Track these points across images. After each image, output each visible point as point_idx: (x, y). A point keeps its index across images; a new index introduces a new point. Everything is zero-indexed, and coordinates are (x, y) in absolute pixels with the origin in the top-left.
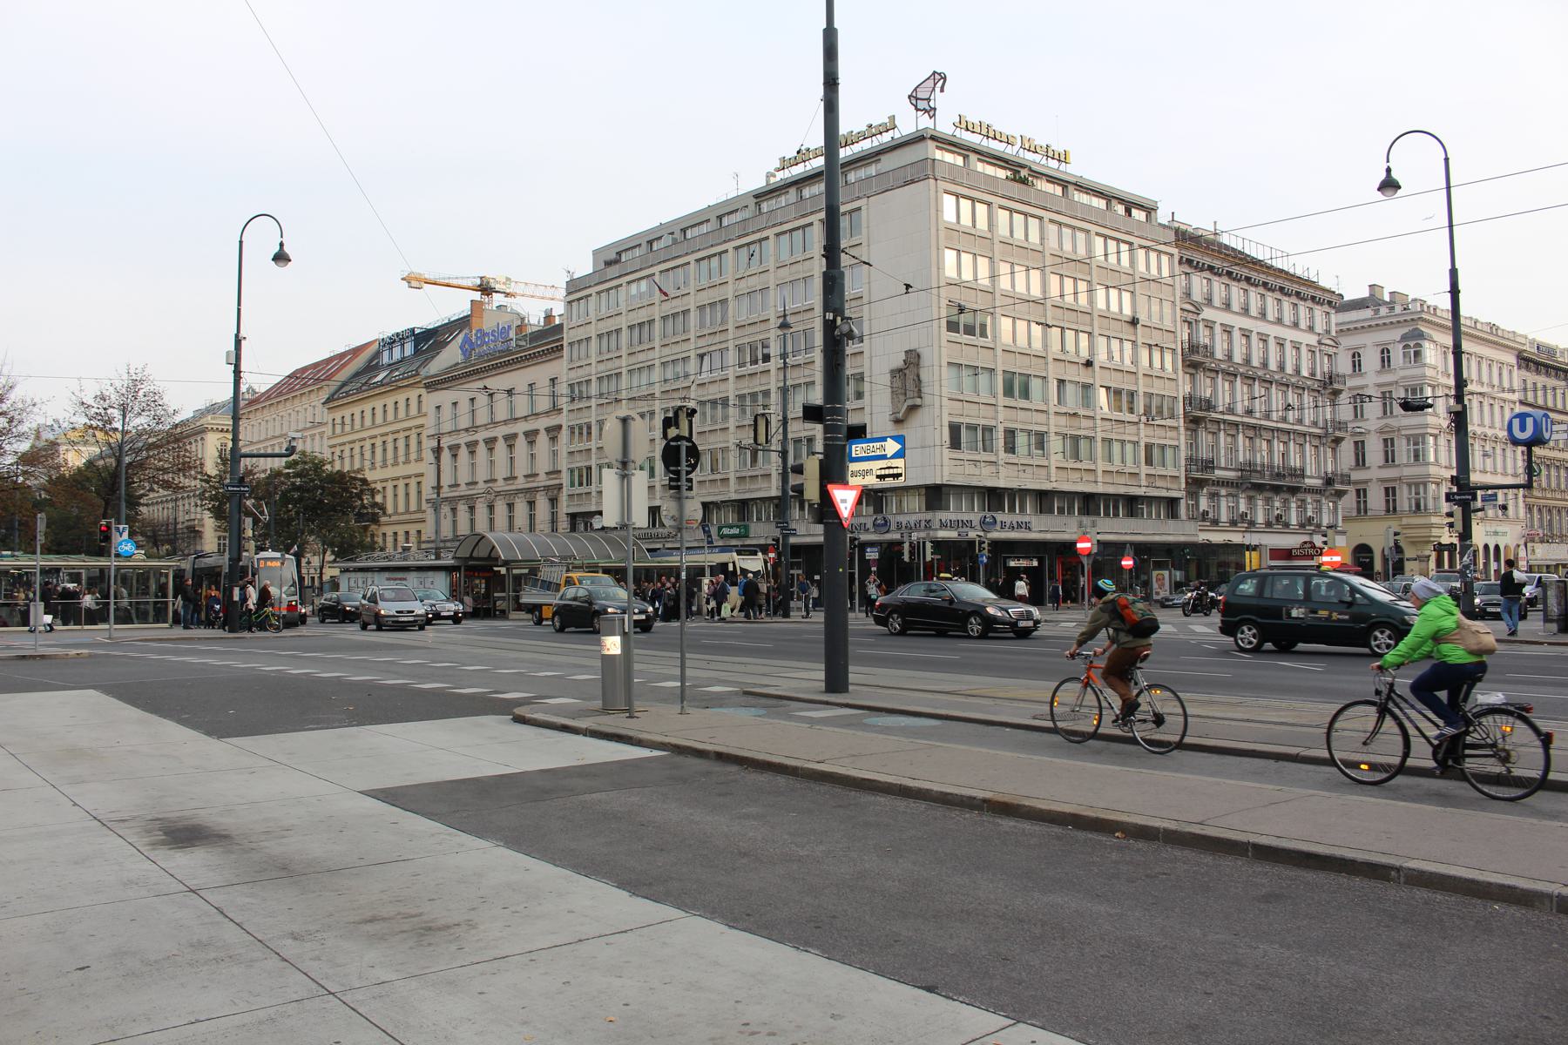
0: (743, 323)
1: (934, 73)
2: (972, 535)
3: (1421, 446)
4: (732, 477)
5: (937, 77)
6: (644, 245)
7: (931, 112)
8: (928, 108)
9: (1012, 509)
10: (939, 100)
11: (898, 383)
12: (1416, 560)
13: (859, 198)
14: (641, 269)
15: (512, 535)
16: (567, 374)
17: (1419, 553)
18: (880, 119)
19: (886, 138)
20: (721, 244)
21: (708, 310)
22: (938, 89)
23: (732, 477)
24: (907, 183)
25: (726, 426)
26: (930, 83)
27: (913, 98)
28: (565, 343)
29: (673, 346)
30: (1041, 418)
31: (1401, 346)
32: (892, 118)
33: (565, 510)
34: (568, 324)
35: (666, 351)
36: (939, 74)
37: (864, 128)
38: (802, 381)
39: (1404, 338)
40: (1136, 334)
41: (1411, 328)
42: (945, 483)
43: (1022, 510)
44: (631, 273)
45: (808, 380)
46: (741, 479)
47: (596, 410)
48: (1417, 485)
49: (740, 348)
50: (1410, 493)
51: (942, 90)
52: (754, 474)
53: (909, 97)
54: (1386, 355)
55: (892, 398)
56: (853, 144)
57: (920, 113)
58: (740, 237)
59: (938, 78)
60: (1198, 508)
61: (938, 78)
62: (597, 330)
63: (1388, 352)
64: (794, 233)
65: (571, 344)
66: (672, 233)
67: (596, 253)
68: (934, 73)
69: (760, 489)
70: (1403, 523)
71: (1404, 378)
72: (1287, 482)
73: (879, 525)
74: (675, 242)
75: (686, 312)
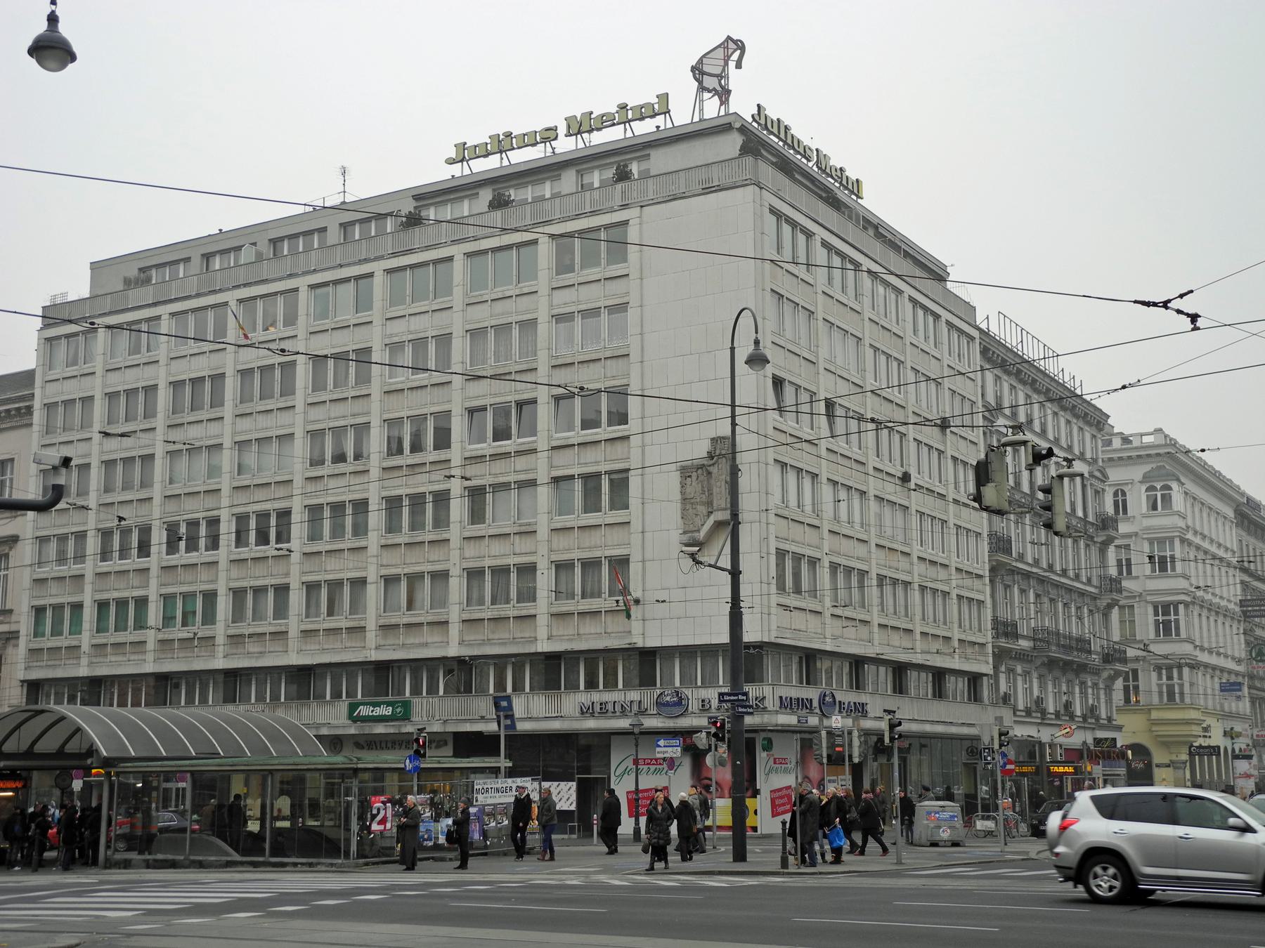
0: (400, 386)
1: (729, 38)
2: (813, 721)
3: (1172, 618)
4: (371, 625)
5: (732, 45)
6: (196, 261)
7: (724, 94)
8: (719, 88)
9: (190, 701)
10: (735, 78)
11: (694, 487)
12: (1168, 766)
13: (625, 207)
14: (198, 295)
15: (202, 711)
16: (234, 423)
17: (1174, 758)
18: (646, 96)
19: (644, 128)
20: (281, 279)
21: (61, 409)
22: (732, 65)
23: (371, 625)
24: (708, 190)
25: (362, 543)
26: (720, 53)
27: (698, 71)
28: (37, 404)
29: (260, 418)
30: (861, 550)
31: (1144, 488)
32: (664, 98)
33: (21, 675)
34: (44, 374)
35: (245, 424)
36: (735, 42)
37: (614, 109)
38: (512, 478)
39: (1146, 478)
40: (944, 443)
41: (1154, 466)
42: (773, 640)
43: (204, 701)
44: (177, 300)
45: (523, 477)
46: (386, 628)
47: (163, 505)
48: (1169, 668)
49: (316, 435)
50: (1160, 678)
51: (739, 66)
52: (259, 630)
53: (693, 69)
54: (1120, 498)
55: (684, 509)
56: (590, 131)
57: (707, 95)
58: (395, 255)
59: (733, 47)
60: (998, 689)
61: (733, 47)
62: (104, 385)
63: (1124, 494)
64: (341, 288)
65: (50, 407)
66: (254, 244)
67: (95, 266)
68: (729, 38)
69: (426, 645)
70: (1152, 717)
71: (1148, 528)
72: (1075, 657)
73: (667, 704)
74: (260, 258)
75: (87, 400)
